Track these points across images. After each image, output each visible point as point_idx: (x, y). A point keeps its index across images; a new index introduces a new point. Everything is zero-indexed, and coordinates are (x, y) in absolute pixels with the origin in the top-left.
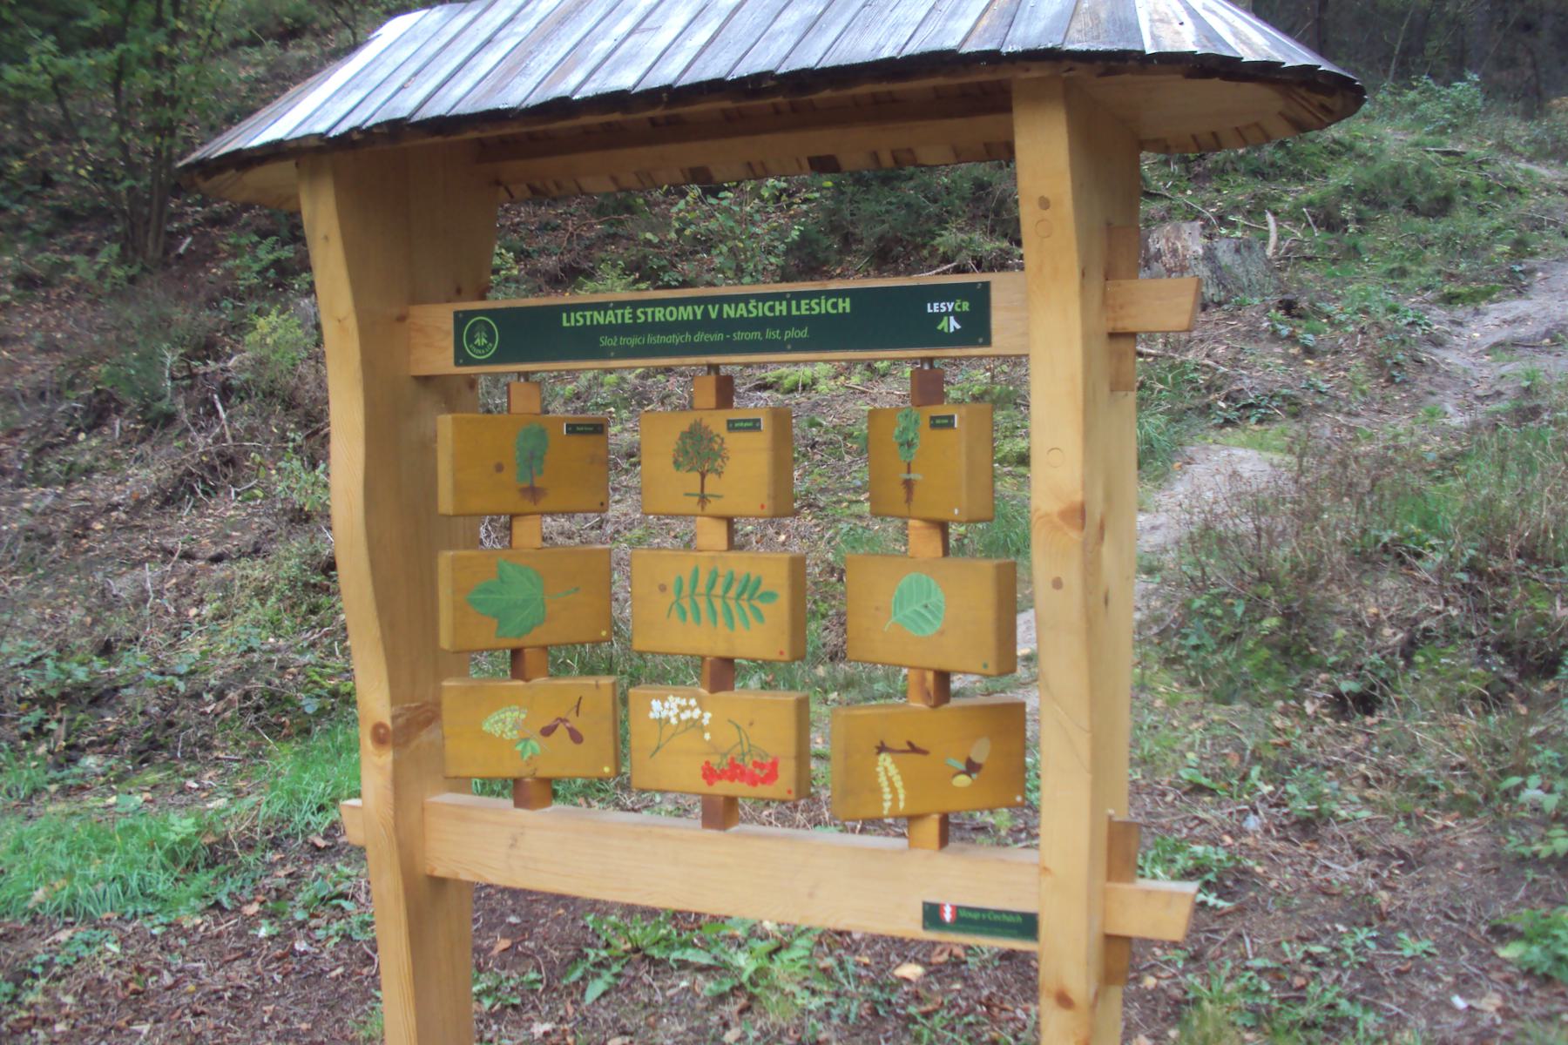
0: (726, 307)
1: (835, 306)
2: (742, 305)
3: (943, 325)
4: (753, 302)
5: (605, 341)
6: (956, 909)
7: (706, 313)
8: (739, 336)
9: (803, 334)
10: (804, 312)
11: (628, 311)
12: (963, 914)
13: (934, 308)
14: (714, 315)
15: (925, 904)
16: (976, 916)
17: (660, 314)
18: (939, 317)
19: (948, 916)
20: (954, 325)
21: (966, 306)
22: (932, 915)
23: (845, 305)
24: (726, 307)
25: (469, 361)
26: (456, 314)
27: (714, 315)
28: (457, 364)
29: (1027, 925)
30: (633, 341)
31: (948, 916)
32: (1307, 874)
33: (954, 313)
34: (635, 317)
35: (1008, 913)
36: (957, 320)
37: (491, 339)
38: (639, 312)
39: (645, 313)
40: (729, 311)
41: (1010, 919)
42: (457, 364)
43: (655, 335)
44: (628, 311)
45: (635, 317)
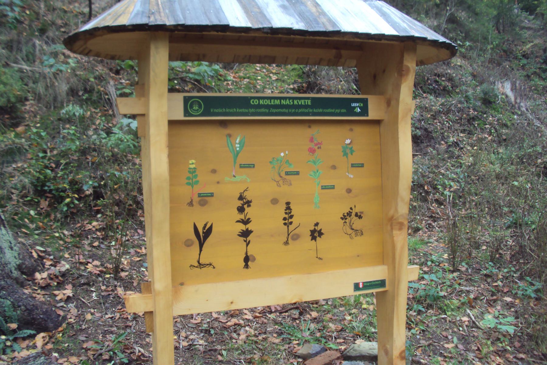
0: (282, 101)
3: (356, 110)
4: (288, 100)
6: (363, 283)
10: (272, 103)
12: (365, 284)
13: (353, 105)
16: (368, 284)
18: (355, 108)
19: (361, 286)
20: (359, 110)
21: (362, 105)
22: (357, 287)
24: (282, 101)
26: (185, 97)
31: (361, 286)
33: (359, 106)
35: (377, 281)
37: (200, 106)
42: (185, 116)
43: (251, 109)
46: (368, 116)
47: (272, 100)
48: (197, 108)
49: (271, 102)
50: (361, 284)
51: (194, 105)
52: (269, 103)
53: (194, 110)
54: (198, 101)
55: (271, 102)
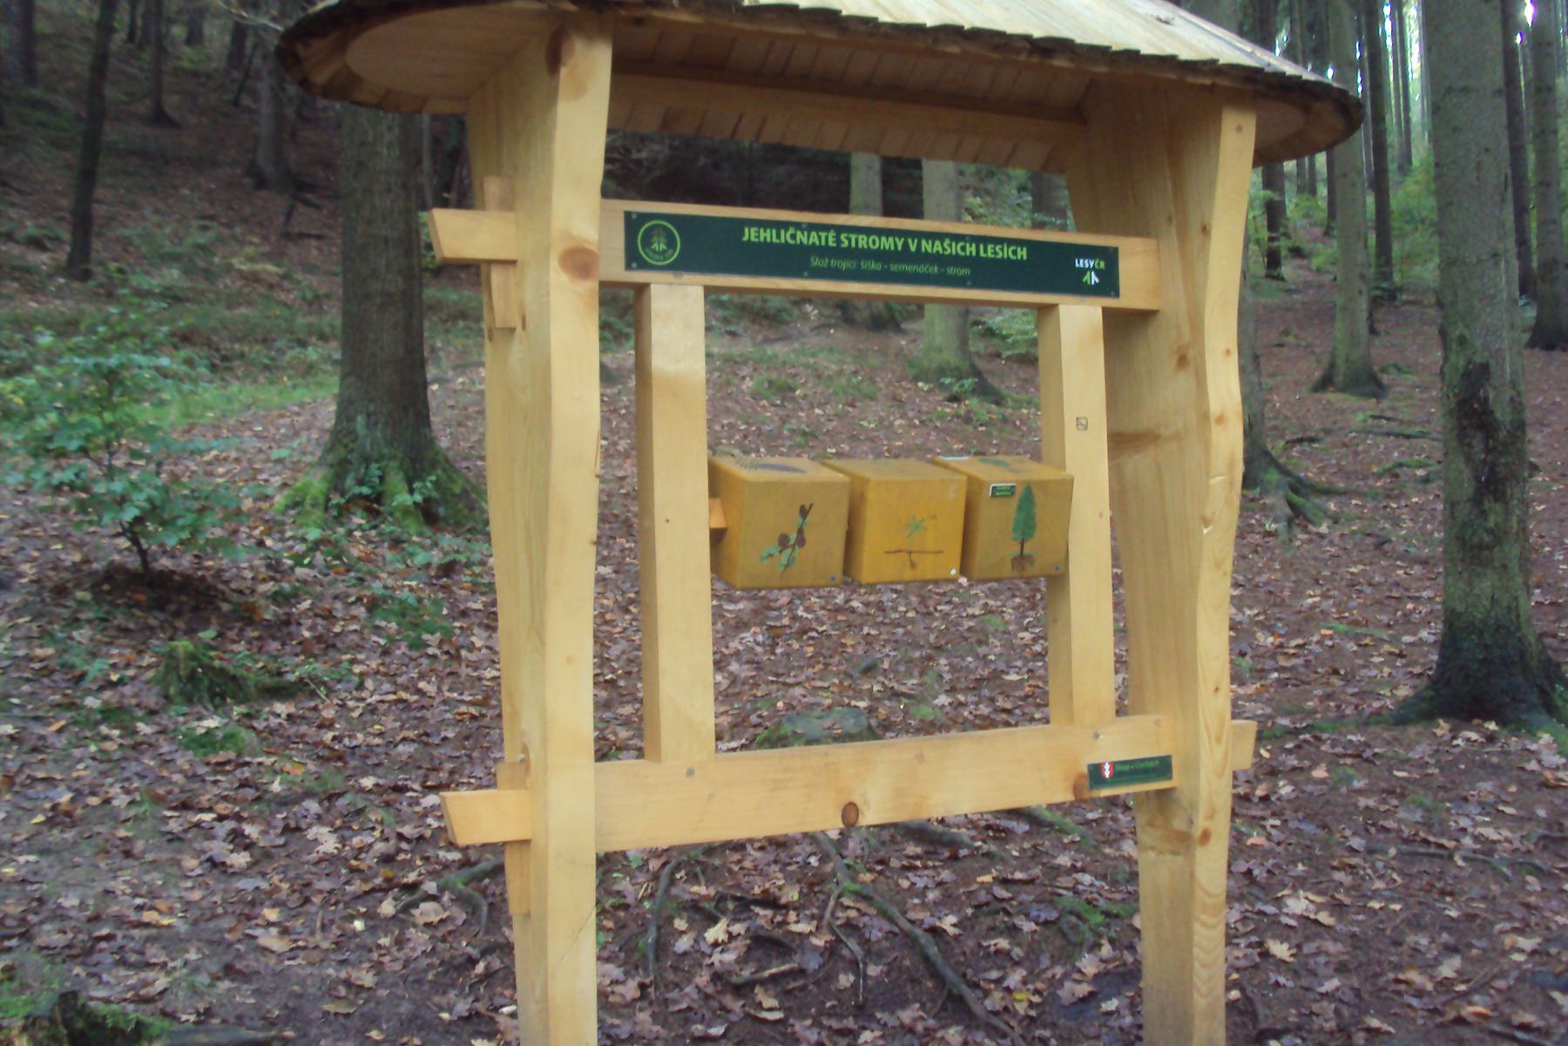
0: (924, 242)
1: (1015, 252)
2: (937, 243)
3: (1086, 278)
4: (947, 242)
5: (816, 262)
6: (1113, 764)
7: (906, 245)
8: (951, 271)
9: (965, 271)
10: (990, 255)
11: (832, 234)
12: (1119, 768)
13: (1081, 263)
14: (913, 248)
15: (1169, 757)
16: (1127, 768)
17: (863, 241)
18: (1083, 271)
19: (1107, 774)
20: (1095, 279)
21: (1102, 265)
23: (1023, 253)
24: (924, 242)
25: (644, 266)
27: (913, 248)
28: (628, 267)
29: (1162, 767)
30: (844, 265)
31: (1107, 774)
32: (372, 710)
34: (838, 241)
35: (1143, 760)
36: (1097, 275)
37: (671, 243)
38: (843, 237)
39: (849, 240)
40: (926, 246)
41: (1151, 764)
44: (832, 234)
45: (838, 241)
46: (1117, 295)
47: (990, 247)
48: (663, 247)
49: (778, 236)
50: (1107, 767)
51: (655, 239)
52: (775, 240)
53: (654, 251)
54: (665, 228)
55: (778, 236)
